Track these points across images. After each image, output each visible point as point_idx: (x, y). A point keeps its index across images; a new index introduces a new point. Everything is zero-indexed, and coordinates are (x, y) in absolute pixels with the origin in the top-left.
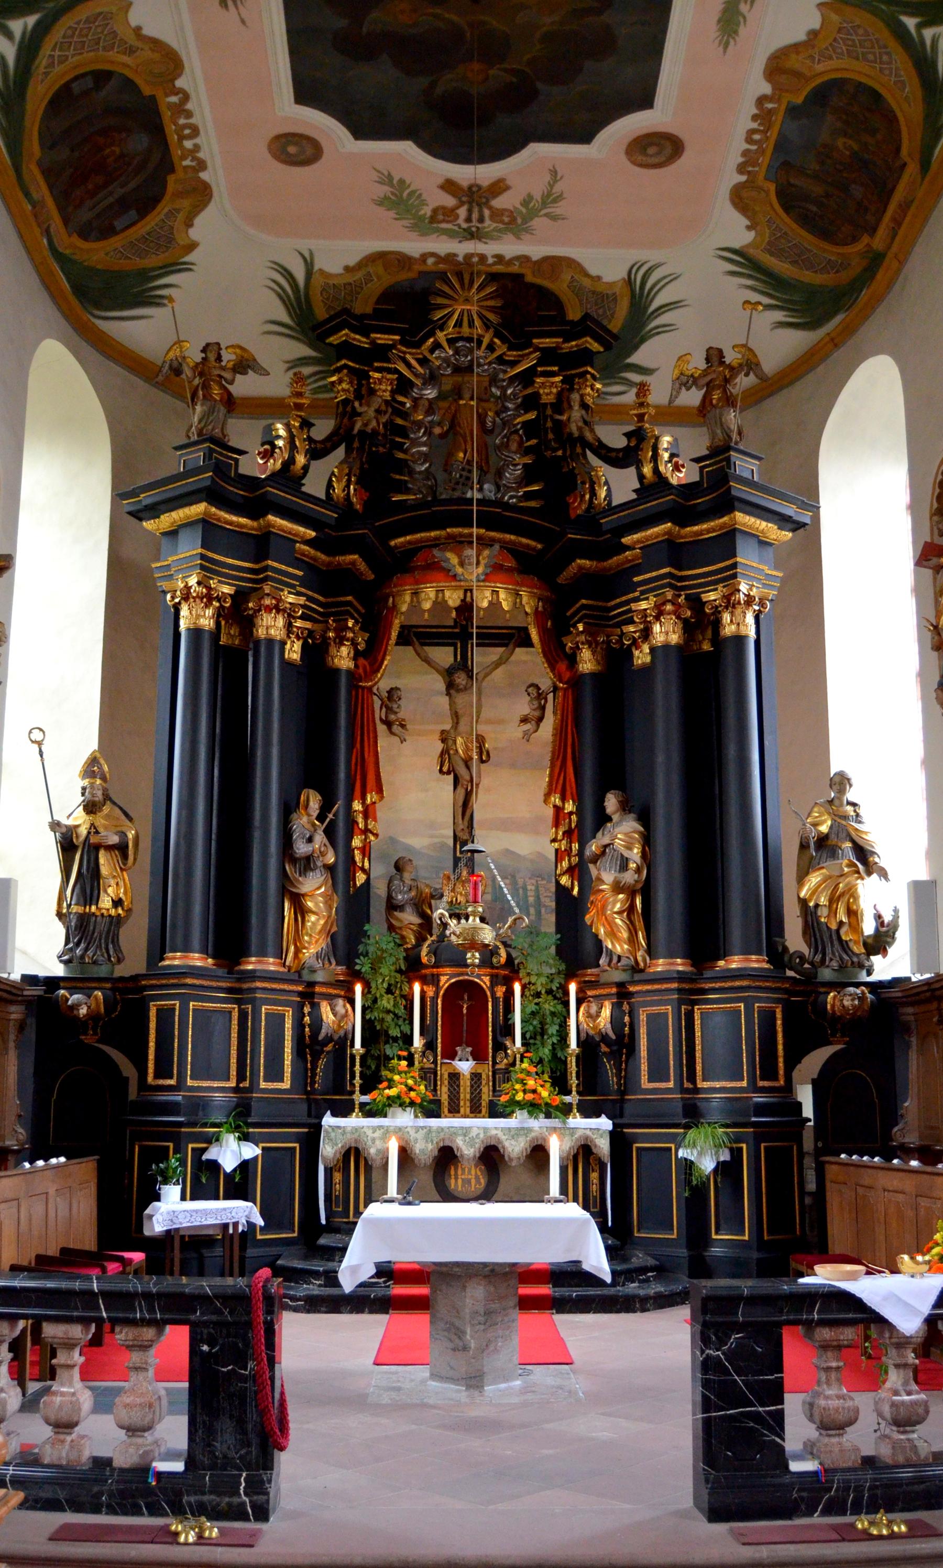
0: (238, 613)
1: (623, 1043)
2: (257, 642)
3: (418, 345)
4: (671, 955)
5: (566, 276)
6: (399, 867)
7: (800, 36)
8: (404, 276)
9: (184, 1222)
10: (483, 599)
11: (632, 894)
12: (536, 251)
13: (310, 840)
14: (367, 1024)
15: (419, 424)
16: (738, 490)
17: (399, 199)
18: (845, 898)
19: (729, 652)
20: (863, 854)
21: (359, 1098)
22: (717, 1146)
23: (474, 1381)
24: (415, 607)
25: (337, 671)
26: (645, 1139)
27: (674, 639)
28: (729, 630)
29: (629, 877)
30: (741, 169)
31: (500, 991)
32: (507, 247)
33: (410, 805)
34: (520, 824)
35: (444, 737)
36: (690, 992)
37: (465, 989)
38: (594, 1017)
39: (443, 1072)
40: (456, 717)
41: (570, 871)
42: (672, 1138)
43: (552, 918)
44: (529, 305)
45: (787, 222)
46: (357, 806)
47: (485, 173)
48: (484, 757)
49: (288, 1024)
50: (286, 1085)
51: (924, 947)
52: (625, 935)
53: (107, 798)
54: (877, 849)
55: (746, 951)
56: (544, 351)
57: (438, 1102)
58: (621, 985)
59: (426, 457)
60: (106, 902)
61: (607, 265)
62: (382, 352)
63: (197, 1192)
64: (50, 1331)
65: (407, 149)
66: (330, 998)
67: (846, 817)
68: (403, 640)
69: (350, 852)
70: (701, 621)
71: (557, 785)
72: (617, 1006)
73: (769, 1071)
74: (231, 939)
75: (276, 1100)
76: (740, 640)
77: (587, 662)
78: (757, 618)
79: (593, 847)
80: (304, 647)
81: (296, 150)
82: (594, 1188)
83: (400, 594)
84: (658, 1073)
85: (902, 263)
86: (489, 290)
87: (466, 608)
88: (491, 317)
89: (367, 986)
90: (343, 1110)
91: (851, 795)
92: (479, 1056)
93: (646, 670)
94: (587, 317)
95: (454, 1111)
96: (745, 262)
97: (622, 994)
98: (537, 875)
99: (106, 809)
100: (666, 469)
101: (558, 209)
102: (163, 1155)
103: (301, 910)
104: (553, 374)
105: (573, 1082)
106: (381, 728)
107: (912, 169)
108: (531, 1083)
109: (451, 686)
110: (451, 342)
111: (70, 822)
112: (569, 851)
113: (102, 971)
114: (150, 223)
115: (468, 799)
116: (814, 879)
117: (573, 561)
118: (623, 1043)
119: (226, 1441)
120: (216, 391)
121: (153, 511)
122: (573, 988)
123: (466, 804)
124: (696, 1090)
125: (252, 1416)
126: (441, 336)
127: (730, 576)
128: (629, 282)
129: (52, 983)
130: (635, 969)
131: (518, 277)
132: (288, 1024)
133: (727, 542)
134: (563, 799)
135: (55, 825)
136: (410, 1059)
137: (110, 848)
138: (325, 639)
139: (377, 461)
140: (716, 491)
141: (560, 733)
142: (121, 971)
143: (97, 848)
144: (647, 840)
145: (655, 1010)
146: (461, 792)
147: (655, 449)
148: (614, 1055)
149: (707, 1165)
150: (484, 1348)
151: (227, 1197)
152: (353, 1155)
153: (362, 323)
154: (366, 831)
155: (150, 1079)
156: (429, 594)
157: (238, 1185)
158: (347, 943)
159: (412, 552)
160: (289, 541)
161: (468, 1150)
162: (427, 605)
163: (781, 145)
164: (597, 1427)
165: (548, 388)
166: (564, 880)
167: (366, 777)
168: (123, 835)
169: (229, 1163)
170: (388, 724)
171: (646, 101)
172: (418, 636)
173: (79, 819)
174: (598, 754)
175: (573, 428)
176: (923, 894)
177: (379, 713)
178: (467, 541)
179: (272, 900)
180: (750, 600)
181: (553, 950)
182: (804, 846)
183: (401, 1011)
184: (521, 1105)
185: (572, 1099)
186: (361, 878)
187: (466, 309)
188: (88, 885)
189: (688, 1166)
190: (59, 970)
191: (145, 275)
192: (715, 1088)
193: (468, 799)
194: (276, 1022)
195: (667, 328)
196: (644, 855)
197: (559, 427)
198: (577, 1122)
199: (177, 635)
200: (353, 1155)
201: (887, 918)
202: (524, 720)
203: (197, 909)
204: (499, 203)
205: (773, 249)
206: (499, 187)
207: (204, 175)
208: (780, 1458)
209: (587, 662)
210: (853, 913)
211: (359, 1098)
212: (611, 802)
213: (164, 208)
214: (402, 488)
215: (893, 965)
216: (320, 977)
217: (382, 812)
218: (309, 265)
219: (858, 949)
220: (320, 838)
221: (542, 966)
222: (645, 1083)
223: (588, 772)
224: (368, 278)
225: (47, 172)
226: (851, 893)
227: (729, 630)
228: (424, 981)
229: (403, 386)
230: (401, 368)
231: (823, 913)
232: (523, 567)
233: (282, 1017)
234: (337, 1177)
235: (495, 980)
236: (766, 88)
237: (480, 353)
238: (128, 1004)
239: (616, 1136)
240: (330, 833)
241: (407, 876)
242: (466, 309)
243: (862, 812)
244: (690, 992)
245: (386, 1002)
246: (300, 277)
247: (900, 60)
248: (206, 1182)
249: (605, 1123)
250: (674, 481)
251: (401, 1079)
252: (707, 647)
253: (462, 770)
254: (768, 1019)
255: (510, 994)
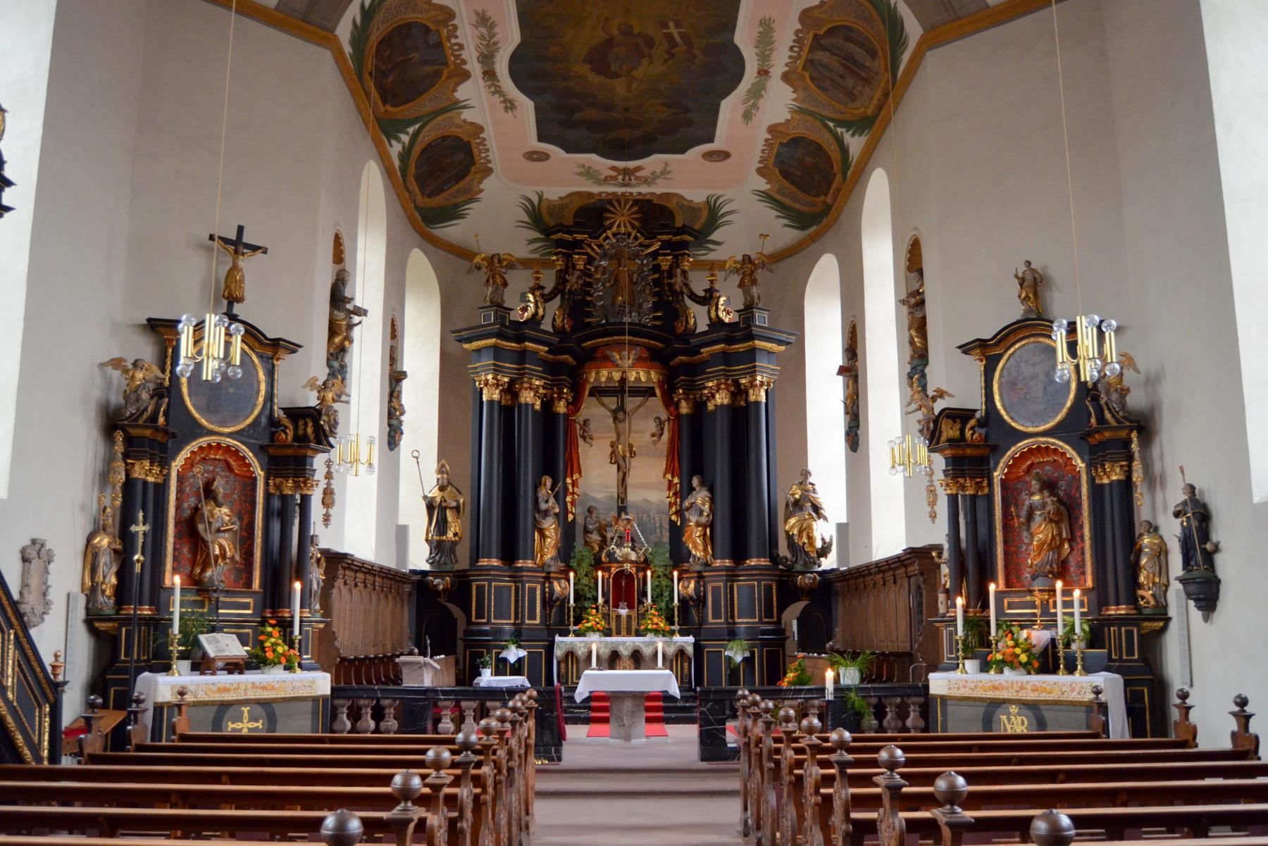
0: (511, 390)
1: (700, 600)
2: (520, 405)
3: (598, 238)
4: (723, 558)
5: (675, 200)
6: (590, 511)
7: (782, 121)
8: (591, 201)
9: (494, 685)
10: (632, 376)
11: (705, 527)
12: (659, 191)
13: (547, 502)
14: (576, 592)
15: (598, 280)
16: (755, 331)
17: (589, 173)
18: (806, 530)
19: (752, 408)
20: (817, 509)
21: (572, 628)
22: (744, 651)
23: (628, 738)
24: (597, 379)
25: (558, 414)
26: (710, 647)
27: (726, 401)
28: (752, 398)
29: (703, 520)
30: (760, 162)
31: (641, 574)
32: (644, 189)
33: (595, 476)
34: (651, 485)
35: (613, 445)
36: (732, 576)
37: (621, 574)
38: (686, 588)
39: (613, 615)
40: (618, 435)
41: (676, 513)
42: (722, 646)
43: (668, 534)
44: (655, 216)
45: (786, 183)
46: (569, 481)
47: (632, 164)
48: (633, 454)
49: (538, 593)
50: (538, 621)
51: (842, 556)
52: (701, 548)
53: (449, 483)
54: (824, 506)
55: (758, 557)
56: (662, 241)
57: (610, 630)
58: (699, 572)
59: (601, 298)
60: (450, 535)
61: (696, 195)
62: (577, 244)
63: (498, 672)
64: (489, 704)
65: (594, 156)
66: (558, 579)
67: (808, 491)
68: (591, 394)
69: (565, 503)
70: (739, 392)
71: (670, 469)
72: (697, 583)
73: (769, 613)
74: (510, 550)
75: (532, 629)
76: (758, 403)
77: (684, 408)
78: (767, 391)
79: (686, 504)
80: (542, 402)
81: (534, 156)
82: (686, 670)
83: (590, 373)
84: (716, 615)
85: (839, 214)
86: (635, 209)
87: (623, 380)
88: (636, 223)
89: (576, 573)
90: (565, 633)
91: (811, 480)
92: (630, 607)
93: (714, 412)
94: (684, 226)
95: (619, 633)
96: (767, 197)
97: (700, 577)
98: (660, 512)
99: (449, 489)
100: (722, 315)
101: (669, 176)
102: (481, 655)
103: (543, 537)
104: (668, 255)
105: (676, 619)
106: (581, 441)
107: (839, 177)
108: (655, 620)
109: (615, 419)
110: (614, 235)
111: (430, 495)
112: (675, 503)
113: (448, 568)
114: (461, 184)
115: (624, 472)
116: (793, 521)
117: (679, 357)
118: (700, 600)
119: (547, 737)
120: (499, 281)
121: (469, 340)
122: (676, 573)
123: (624, 480)
124: (735, 623)
125: (556, 730)
126: (609, 233)
127: (752, 373)
128: (708, 202)
129: (424, 574)
130: (707, 564)
131: (650, 201)
132: (538, 593)
133: (751, 355)
134: (673, 476)
135: (425, 497)
136: (597, 609)
137: (451, 508)
138: (552, 398)
139: (577, 306)
140: (743, 330)
141: (671, 442)
142: (456, 567)
143: (445, 508)
144: (712, 501)
145: (715, 584)
146: (621, 474)
147: (717, 305)
148: (697, 606)
149: (738, 658)
150: (630, 726)
151: (511, 674)
152: (570, 654)
153: (568, 229)
154: (573, 493)
155: (473, 619)
156: (605, 373)
157: (516, 669)
158: (566, 552)
159: (595, 348)
160: (536, 353)
161: (625, 652)
162: (603, 379)
163: (778, 155)
164: (674, 748)
165: (665, 262)
166: (674, 518)
167: (573, 465)
168: (458, 501)
169: (512, 659)
170: (584, 438)
171: (711, 139)
172: (598, 392)
173: (435, 493)
174: (689, 459)
175: (677, 287)
176: (842, 528)
177: (579, 432)
178: (622, 343)
179: (530, 532)
180: (762, 383)
181: (667, 555)
182: (787, 505)
183: (592, 585)
184: (650, 631)
185: (676, 627)
186: (570, 517)
187: (621, 222)
188: (442, 526)
189: (729, 659)
190: (427, 567)
191: (456, 206)
192: (743, 622)
193: (624, 472)
194: (533, 590)
195: (728, 223)
196: (711, 508)
197: (671, 285)
198: (677, 638)
199: (481, 402)
200: (570, 654)
201: (828, 540)
202: (653, 435)
203: (494, 537)
204: (638, 174)
205: (779, 192)
206: (639, 169)
207: (465, 67)
208: (724, 743)
209: (684, 408)
210: (810, 538)
211: (572, 628)
212: (695, 481)
213: (469, 178)
214: (589, 315)
215: (829, 563)
216: (553, 569)
217: (580, 482)
218: (541, 197)
219: (814, 555)
220: (552, 500)
221: (664, 557)
222: (711, 620)
223: (685, 464)
224: (572, 202)
225: (416, 178)
226: (810, 528)
227: (752, 398)
228: (603, 570)
229: (590, 260)
230: (589, 251)
231: (796, 538)
232: (654, 357)
233: (535, 589)
234: (563, 665)
235: (638, 570)
236: (799, 26)
237: (631, 240)
238: (461, 586)
239: (697, 646)
240: (556, 497)
241: (594, 515)
242: (621, 222)
243: (817, 487)
244: (732, 576)
245: (585, 581)
246: (536, 201)
247: (828, 136)
248: (502, 667)
249: (691, 639)
250: (727, 320)
251: (593, 619)
252: (743, 403)
253: (621, 462)
254: (768, 589)
255: (645, 577)
